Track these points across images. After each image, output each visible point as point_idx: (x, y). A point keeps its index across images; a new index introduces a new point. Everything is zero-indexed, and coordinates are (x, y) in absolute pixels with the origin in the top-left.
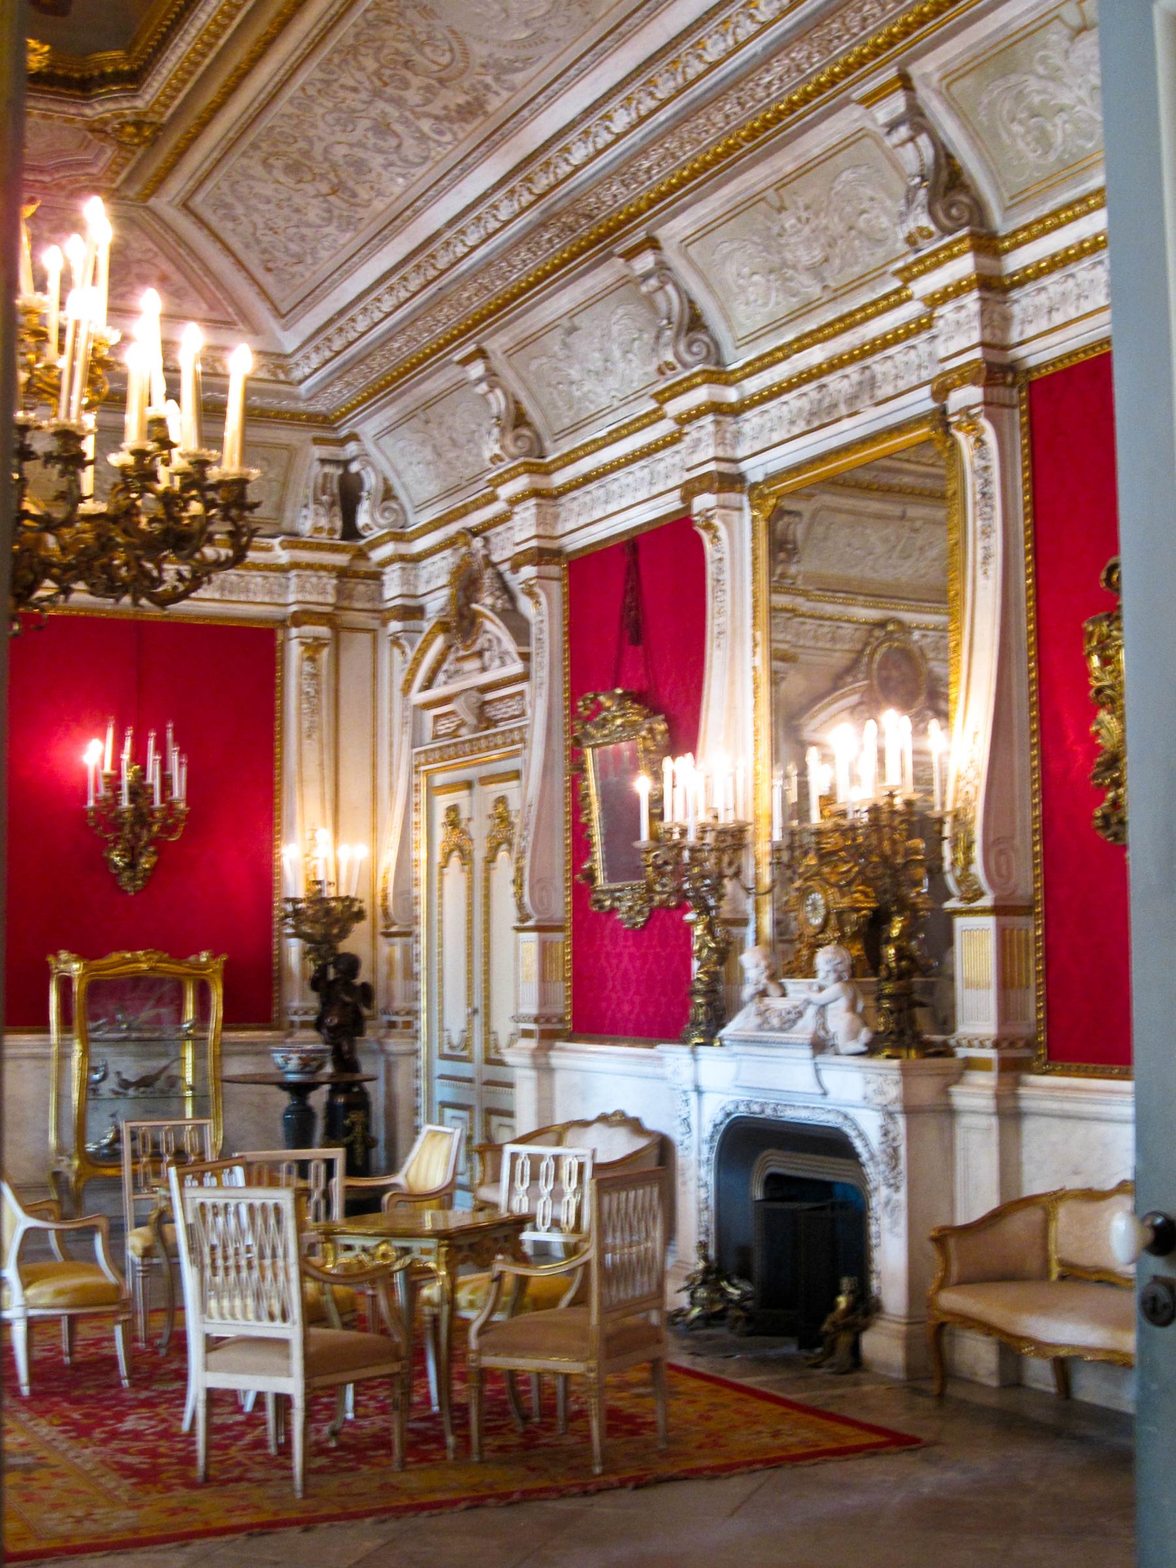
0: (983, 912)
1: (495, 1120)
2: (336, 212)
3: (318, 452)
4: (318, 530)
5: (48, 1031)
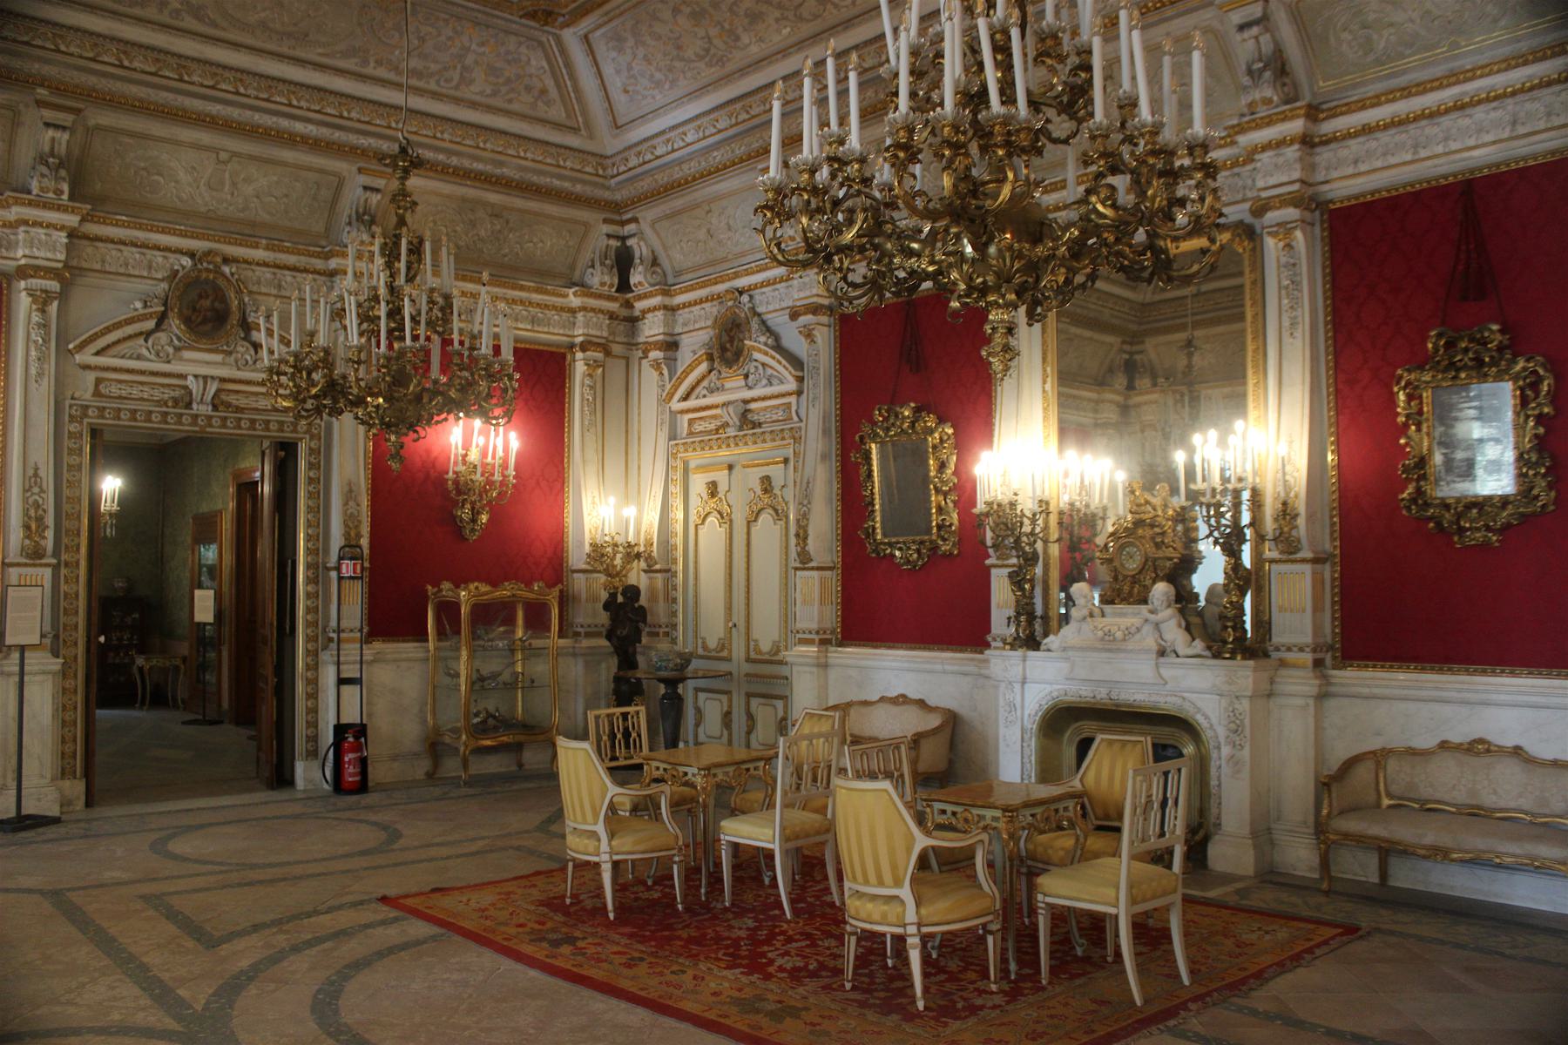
0: (1303, 561)
3: (606, 228)
4: (603, 284)
5: (427, 641)
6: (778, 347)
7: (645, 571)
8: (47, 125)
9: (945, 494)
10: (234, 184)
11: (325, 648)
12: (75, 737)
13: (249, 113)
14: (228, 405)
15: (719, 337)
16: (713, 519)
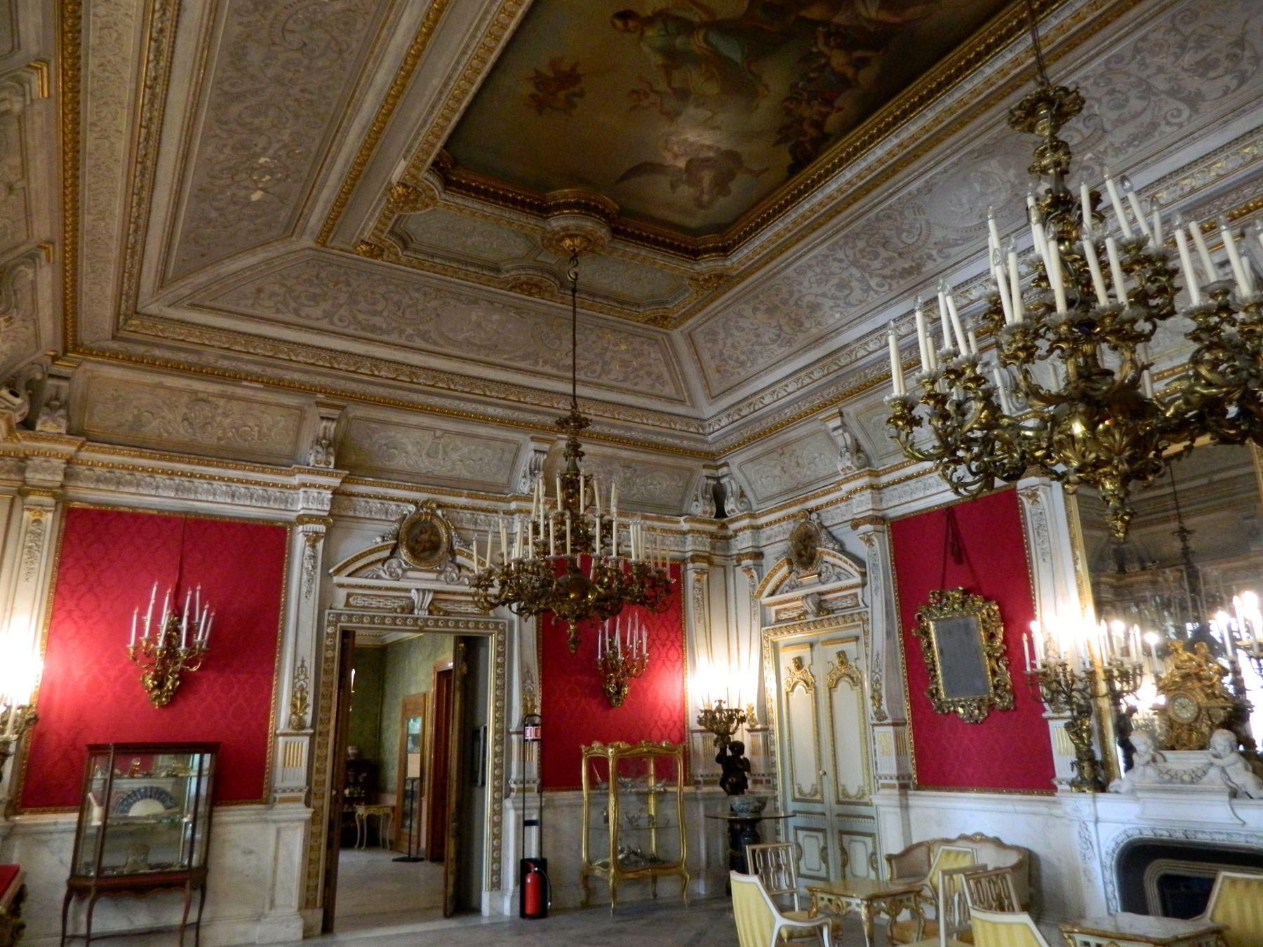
1: (846, 838)
2: (783, 335)
3: (705, 472)
4: (705, 512)
6: (843, 550)
7: (749, 731)
8: (322, 418)
9: (997, 660)
10: (445, 452)
11: (507, 796)
12: (318, 873)
13: (457, 402)
14: (439, 610)
15: (795, 546)
16: (800, 687)
